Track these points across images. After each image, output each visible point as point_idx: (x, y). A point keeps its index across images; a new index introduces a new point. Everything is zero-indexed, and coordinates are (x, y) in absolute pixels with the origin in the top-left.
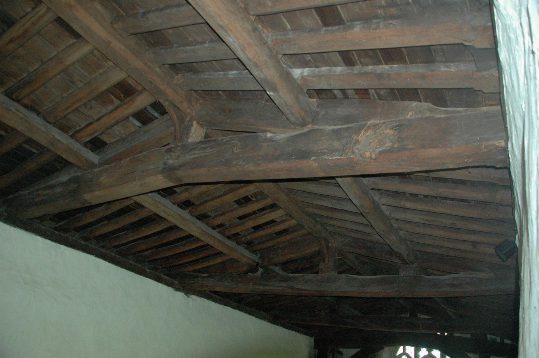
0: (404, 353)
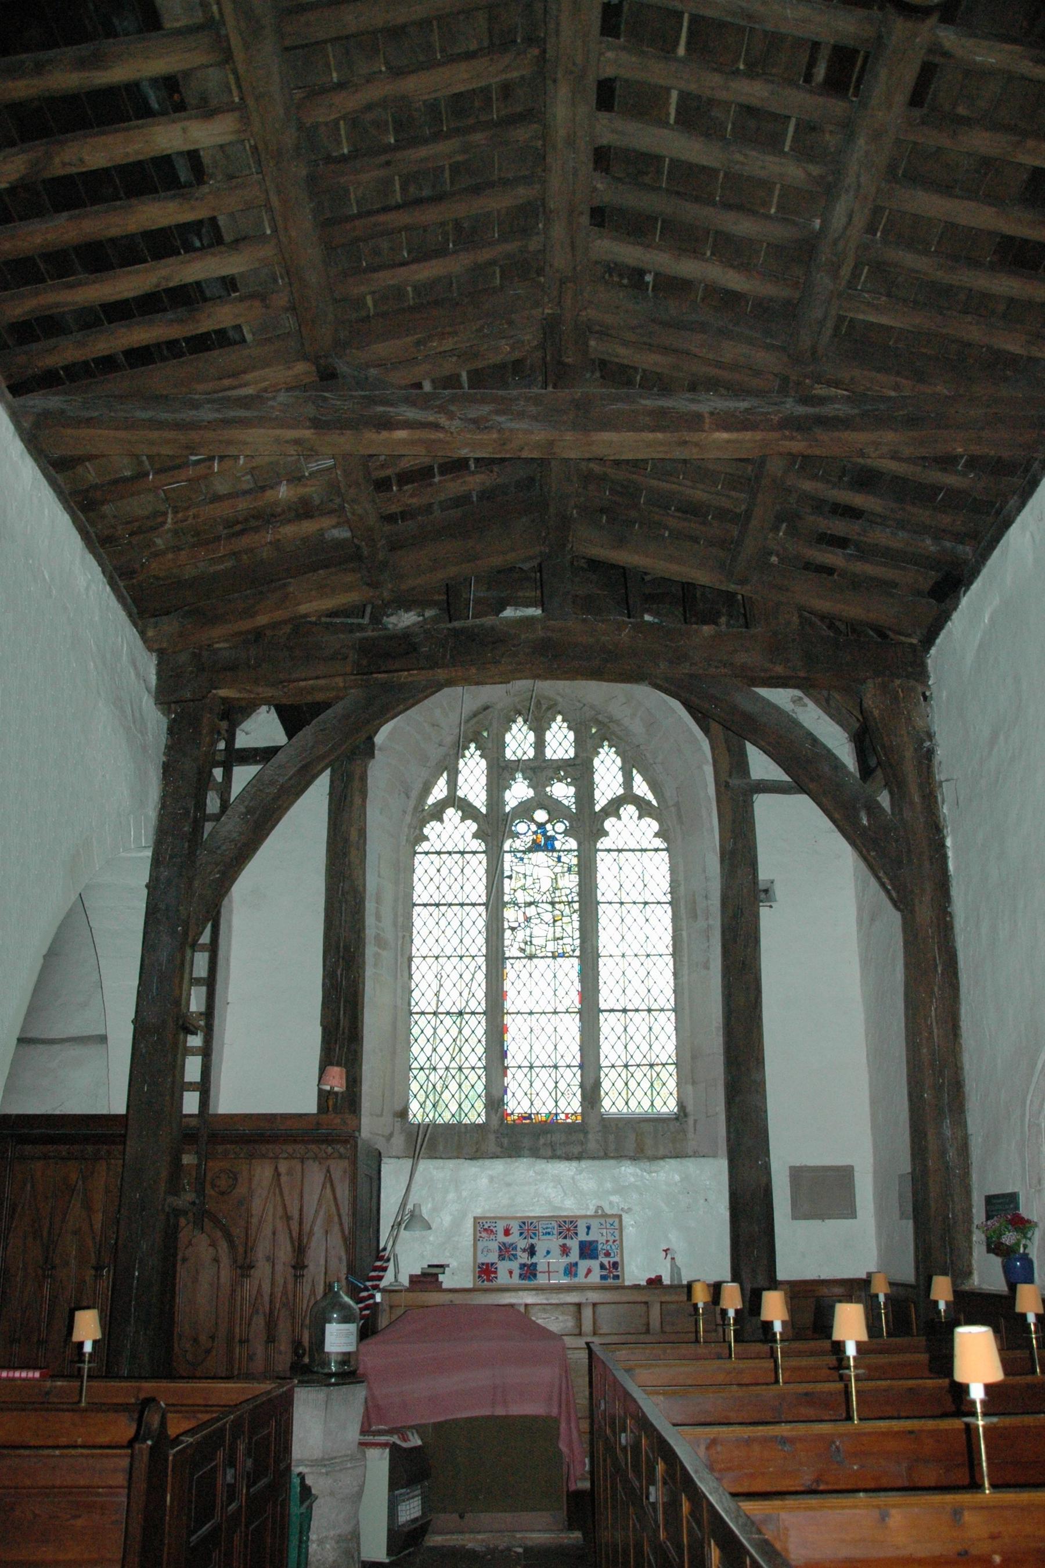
0: (453, 800)
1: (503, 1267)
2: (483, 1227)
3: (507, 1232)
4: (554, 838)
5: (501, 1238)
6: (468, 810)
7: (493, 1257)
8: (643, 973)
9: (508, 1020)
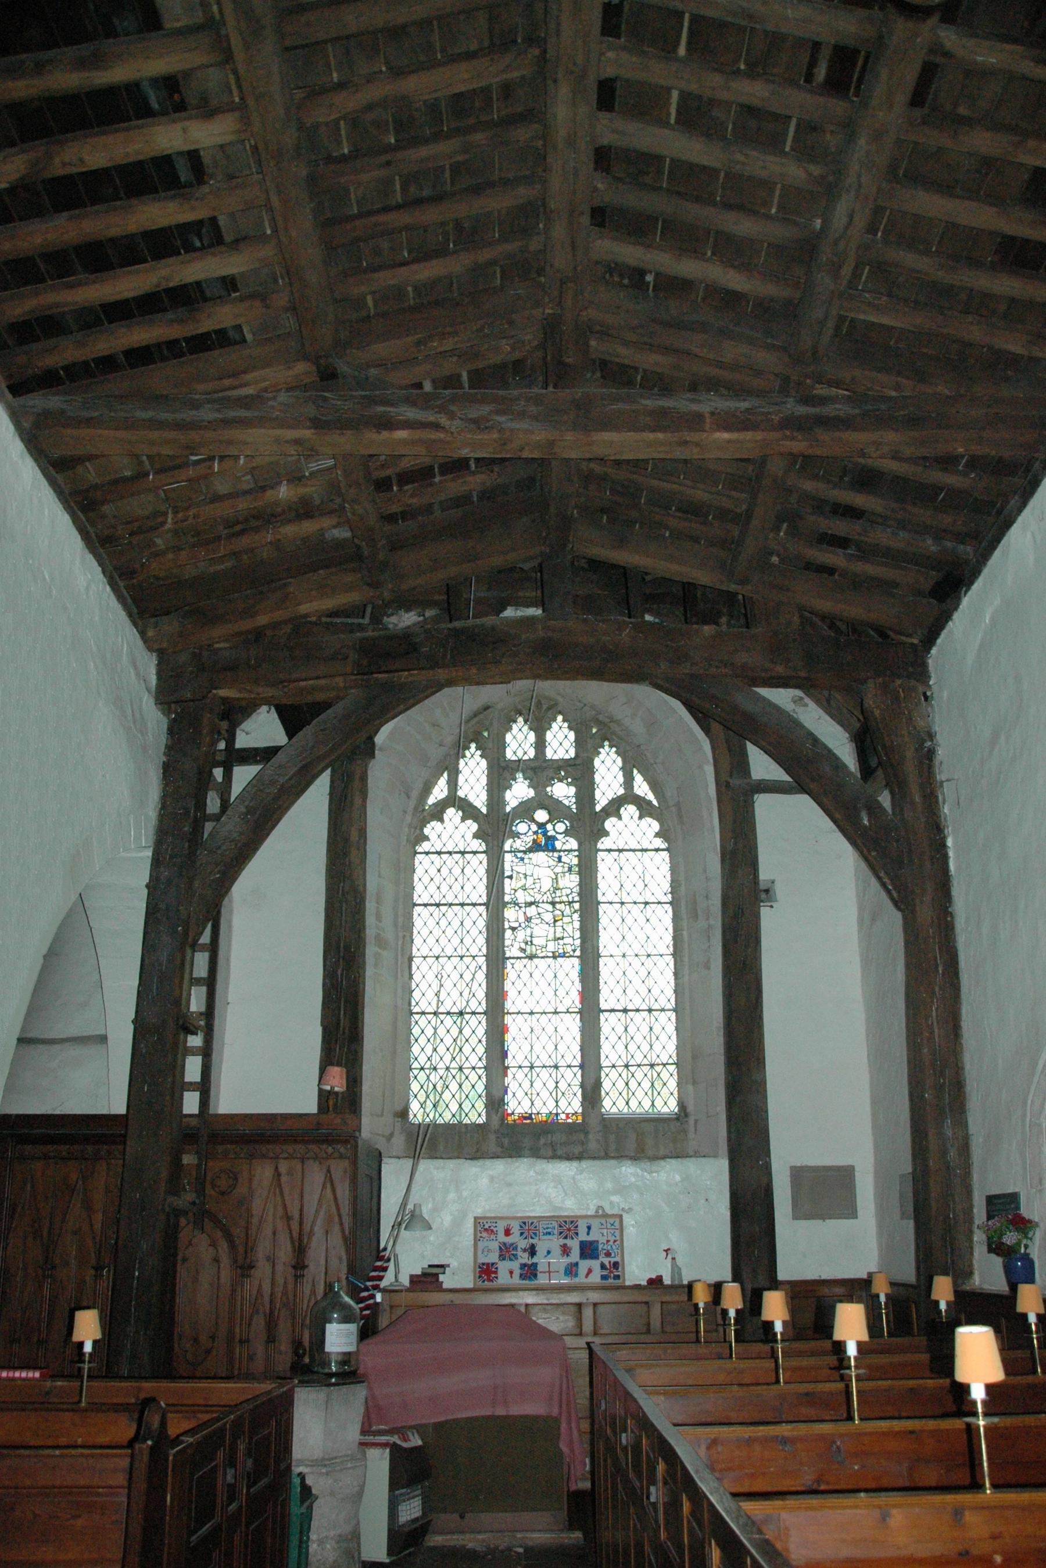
0: (453, 800)
1: (503, 1267)
2: (484, 1227)
3: (507, 1232)
4: (554, 838)
5: (502, 1238)
6: (468, 810)
7: (493, 1257)
8: (643, 973)
9: (508, 1020)
